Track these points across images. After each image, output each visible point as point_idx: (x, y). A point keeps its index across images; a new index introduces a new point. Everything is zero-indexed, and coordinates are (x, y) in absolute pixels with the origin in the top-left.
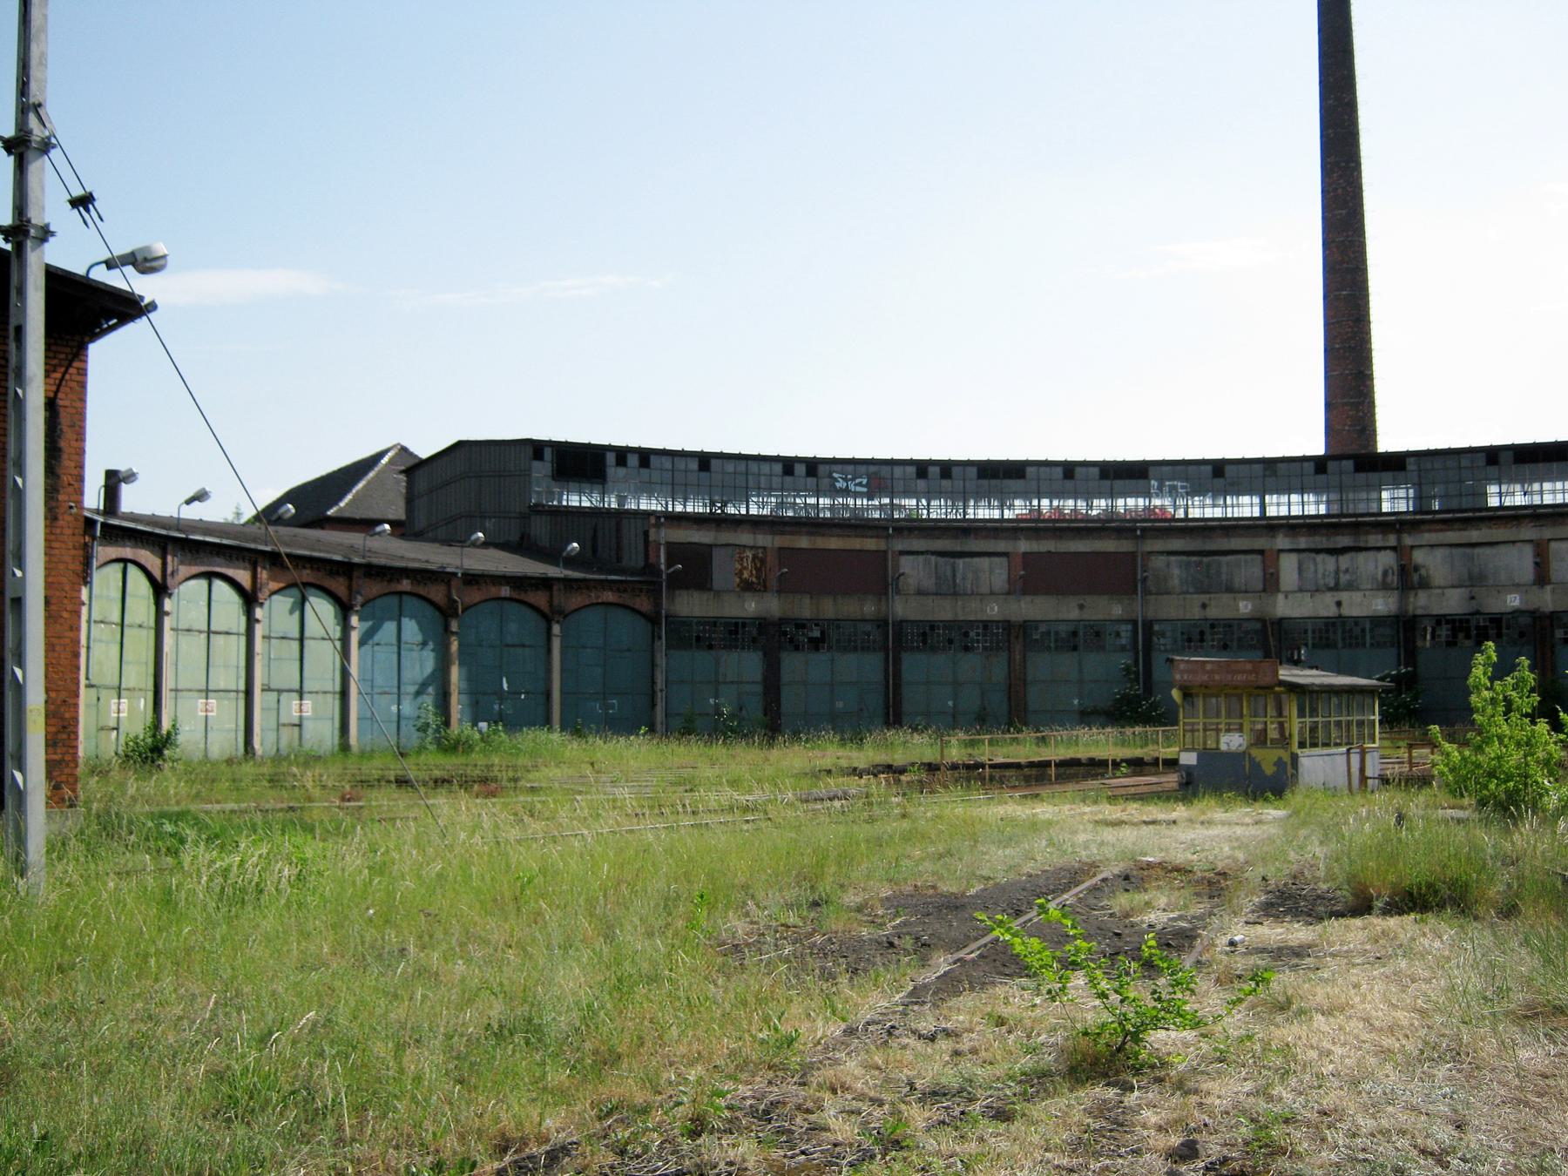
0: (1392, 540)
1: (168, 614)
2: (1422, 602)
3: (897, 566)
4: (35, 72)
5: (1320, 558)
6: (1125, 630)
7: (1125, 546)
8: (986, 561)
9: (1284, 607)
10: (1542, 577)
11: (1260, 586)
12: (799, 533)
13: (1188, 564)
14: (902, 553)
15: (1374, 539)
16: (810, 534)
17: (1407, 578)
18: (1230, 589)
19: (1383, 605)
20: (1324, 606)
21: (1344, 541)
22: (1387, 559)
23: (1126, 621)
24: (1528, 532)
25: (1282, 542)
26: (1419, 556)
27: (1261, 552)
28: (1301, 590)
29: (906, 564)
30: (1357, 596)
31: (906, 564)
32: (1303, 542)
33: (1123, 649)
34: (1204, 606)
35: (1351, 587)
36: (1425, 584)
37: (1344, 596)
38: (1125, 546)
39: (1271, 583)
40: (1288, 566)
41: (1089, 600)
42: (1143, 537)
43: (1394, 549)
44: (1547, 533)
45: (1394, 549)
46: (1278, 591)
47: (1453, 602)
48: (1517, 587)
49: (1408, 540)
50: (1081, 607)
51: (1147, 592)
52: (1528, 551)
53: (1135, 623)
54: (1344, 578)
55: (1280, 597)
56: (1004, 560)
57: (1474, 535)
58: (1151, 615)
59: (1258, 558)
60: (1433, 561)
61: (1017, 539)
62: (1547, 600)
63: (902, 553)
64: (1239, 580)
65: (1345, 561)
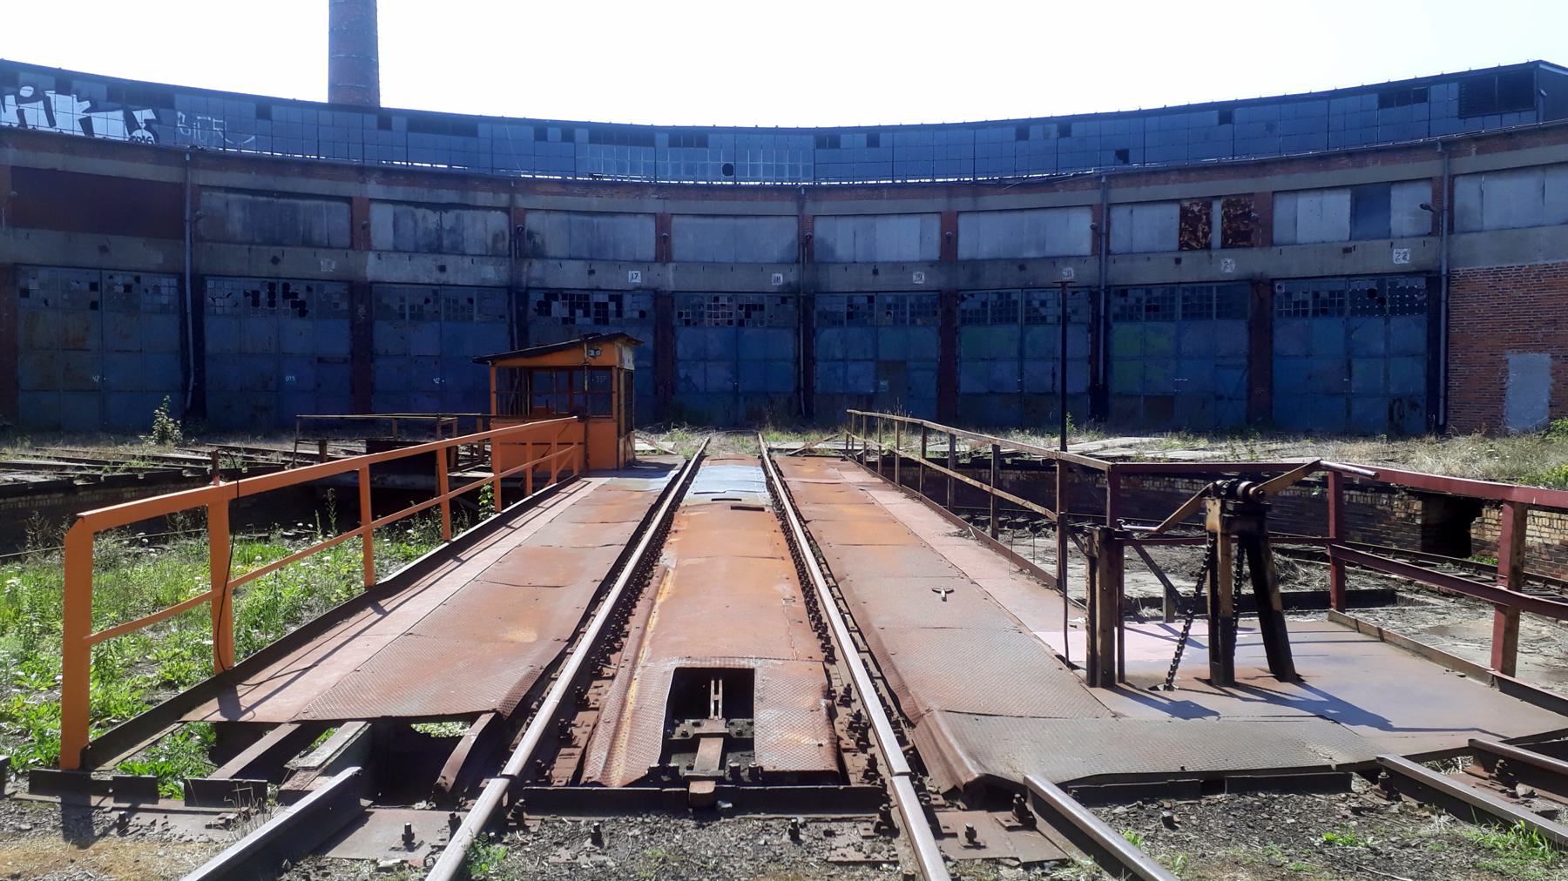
0: (504, 199)
2: (535, 272)
5: (420, 212)
6: (168, 285)
9: (373, 268)
10: (664, 253)
15: (483, 198)
18: (308, 243)
19: (491, 273)
20: (421, 270)
22: (498, 221)
26: (532, 221)
27: (349, 200)
28: (396, 250)
32: (399, 193)
33: (164, 309)
34: (275, 261)
35: (457, 250)
36: (539, 254)
37: (450, 260)
39: (359, 236)
44: (671, 206)
45: (506, 210)
47: (572, 276)
48: (637, 263)
50: (104, 250)
52: (650, 224)
55: (371, 257)
62: (669, 278)
65: (449, 218)
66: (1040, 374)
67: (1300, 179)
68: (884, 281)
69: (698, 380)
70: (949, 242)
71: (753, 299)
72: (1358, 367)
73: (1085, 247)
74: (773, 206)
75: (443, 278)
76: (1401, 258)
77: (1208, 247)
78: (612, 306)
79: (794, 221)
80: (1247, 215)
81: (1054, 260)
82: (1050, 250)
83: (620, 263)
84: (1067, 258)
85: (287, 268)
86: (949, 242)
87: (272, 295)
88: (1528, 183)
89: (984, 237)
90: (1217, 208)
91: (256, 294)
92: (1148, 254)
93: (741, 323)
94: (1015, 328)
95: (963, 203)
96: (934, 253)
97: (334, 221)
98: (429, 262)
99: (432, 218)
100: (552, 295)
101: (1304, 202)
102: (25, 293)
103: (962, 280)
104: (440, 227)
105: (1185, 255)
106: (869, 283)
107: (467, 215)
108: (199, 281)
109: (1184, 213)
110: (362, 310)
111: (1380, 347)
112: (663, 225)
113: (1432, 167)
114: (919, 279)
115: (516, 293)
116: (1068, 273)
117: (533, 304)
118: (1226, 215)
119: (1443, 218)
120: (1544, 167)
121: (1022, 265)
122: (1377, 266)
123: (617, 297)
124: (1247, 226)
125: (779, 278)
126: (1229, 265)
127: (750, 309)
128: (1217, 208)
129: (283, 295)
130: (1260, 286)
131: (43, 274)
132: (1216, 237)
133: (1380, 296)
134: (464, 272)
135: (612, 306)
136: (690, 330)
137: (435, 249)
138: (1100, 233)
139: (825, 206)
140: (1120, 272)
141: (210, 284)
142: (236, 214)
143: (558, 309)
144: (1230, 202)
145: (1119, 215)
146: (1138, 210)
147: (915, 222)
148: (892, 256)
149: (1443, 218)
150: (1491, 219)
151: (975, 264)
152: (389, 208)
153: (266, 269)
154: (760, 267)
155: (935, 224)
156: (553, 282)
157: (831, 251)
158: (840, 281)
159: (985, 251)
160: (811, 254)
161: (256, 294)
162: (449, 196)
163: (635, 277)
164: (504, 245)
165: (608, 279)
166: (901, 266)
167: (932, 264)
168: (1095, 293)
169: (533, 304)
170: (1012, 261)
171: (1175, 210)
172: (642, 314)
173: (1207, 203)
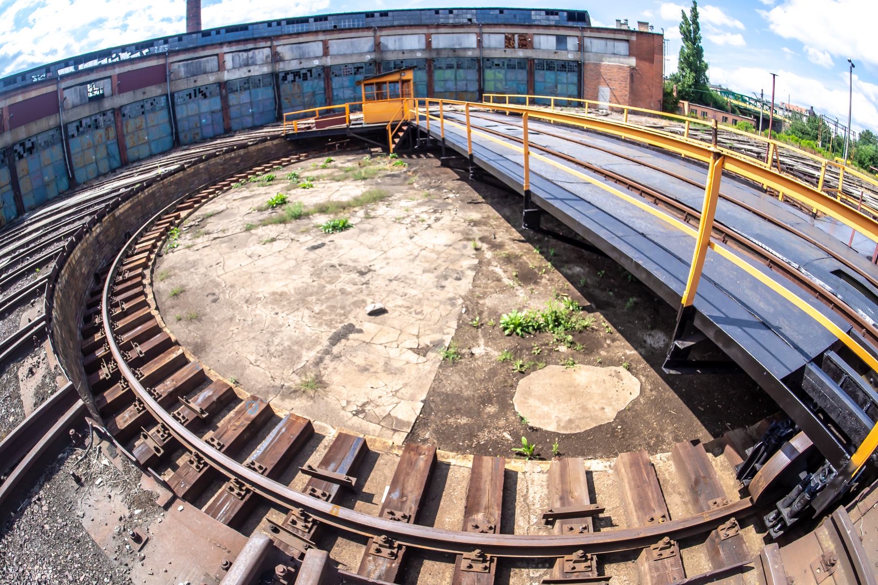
0: (269, 44)
1: (175, 468)
2: (281, 67)
3: (62, 95)
4: (668, 157)
5: (240, 54)
6: (163, 99)
7: (161, 61)
8: (102, 82)
9: (227, 76)
10: (326, 53)
11: (217, 69)
12: (17, 94)
13: (187, 65)
14: (64, 89)
15: (262, 44)
16: (23, 93)
17: (276, 58)
18: (205, 73)
19: (266, 69)
20: (243, 73)
21: (250, 46)
22: (267, 51)
23: (163, 95)
24: (322, 37)
25: (226, 49)
26: (279, 49)
27: (217, 55)
28: (234, 68)
29: (66, 94)
30: (257, 68)
31: (66, 94)
32: (234, 48)
33: (162, 108)
34: (195, 81)
35: (254, 64)
36: (282, 60)
37: (251, 68)
38: (161, 61)
39: (221, 67)
40: (228, 58)
41: (148, 89)
42: (168, 56)
43: (270, 47)
44: (328, 37)
45: (270, 47)
46: (225, 69)
47: (294, 66)
48: (317, 58)
49: (275, 43)
50: (144, 93)
51: (171, 80)
52: (321, 44)
53: (167, 95)
54: (250, 62)
55: (226, 72)
56: (109, 80)
57: (301, 39)
58: (174, 89)
59: (216, 57)
60: (285, 50)
61: (114, 68)
62: (328, 61)
63: (64, 89)
64: (208, 69)
65: (250, 53)
66: (461, 85)
67: (541, 31)
68: (407, 56)
69: (341, 95)
70: (429, 43)
71: (359, 65)
72: (559, 86)
73: (475, 45)
74: (365, 33)
75: (250, 74)
76: (571, 57)
77: (514, 47)
78: (309, 74)
79: (372, 38)
80: (525, 40)
81: (465, 49)
82: (463, 46)
83: (310, 59)
84: (469, 49)
85: (200, 83)
86: (429, 43)
87: (195, 93)
88: (603, 42)
89: (441, 41)
90: (516, 36)
91: (190, 94)
92: (495, 49)
93: (355, 74)
94: (453, 70)
95: (432, 31)
96: (423, 46)
97: (213, 63)
98: (245, 69)
99: (245, 54)
100: (287, 73)
101: (542, 37)
102: (124, 115)
103: (434, 55)
104: (248, 57)
105: (507, 50)
106: (401, 57)
107: (257, 51)
108: (172, 95)
109: (506, 37)
110: (224, 91)
111: (565, 81)
112: (325, 43)
113: (578, 33)
114: (419, 55)
115: (274, 75)
116: (470, 53)
117: (281, 78)
118: (519, 39)
119: (581, 48)
120: (607, 39)
121: (454, 50)
122: (564, 58)
123: (310, 70)
124: (525, 43)
125: (368, 57)
126: (521, 54)
127: (358, 68)
128: (516, 36)
129: (201, 93)
130: (530, 61)
131: (128, 107)
132: (516, 45)
133: (564, 66)
134: (257, 71)
135: (309, 74)
136: (337, 78)
137: (247, 65)
138: (480, 42)
139: (384, 32)
140: (487, 54)
141: (176, 95)
142: (182, 69)
143: (290, 77)
144: (520, 35)
145: (485, 37)
146: (491, 35)
147: (416, 37)
148: (409, 48)
149: (581, 48)
150: (594, 49)
151: (438, 50)
152: (230, 55)
153: (192, 85)
154: (361, 54)
155: (423, 38)
156: (288, 68)
157: (387, 47)
158: (391, 57)
159: (441, 46)
160: (379, 48)
161: (190, 94)
162: (250, 46)
163: (316, 62)
164: (269, 60)
165: (306, 65)
166: (412, 51)
167: (423, 50)
168: (477, 60)
169: (281, 78)
170: (451, 49)
171: (503, 36)
172: (319, 75)
173: (513, 34)
